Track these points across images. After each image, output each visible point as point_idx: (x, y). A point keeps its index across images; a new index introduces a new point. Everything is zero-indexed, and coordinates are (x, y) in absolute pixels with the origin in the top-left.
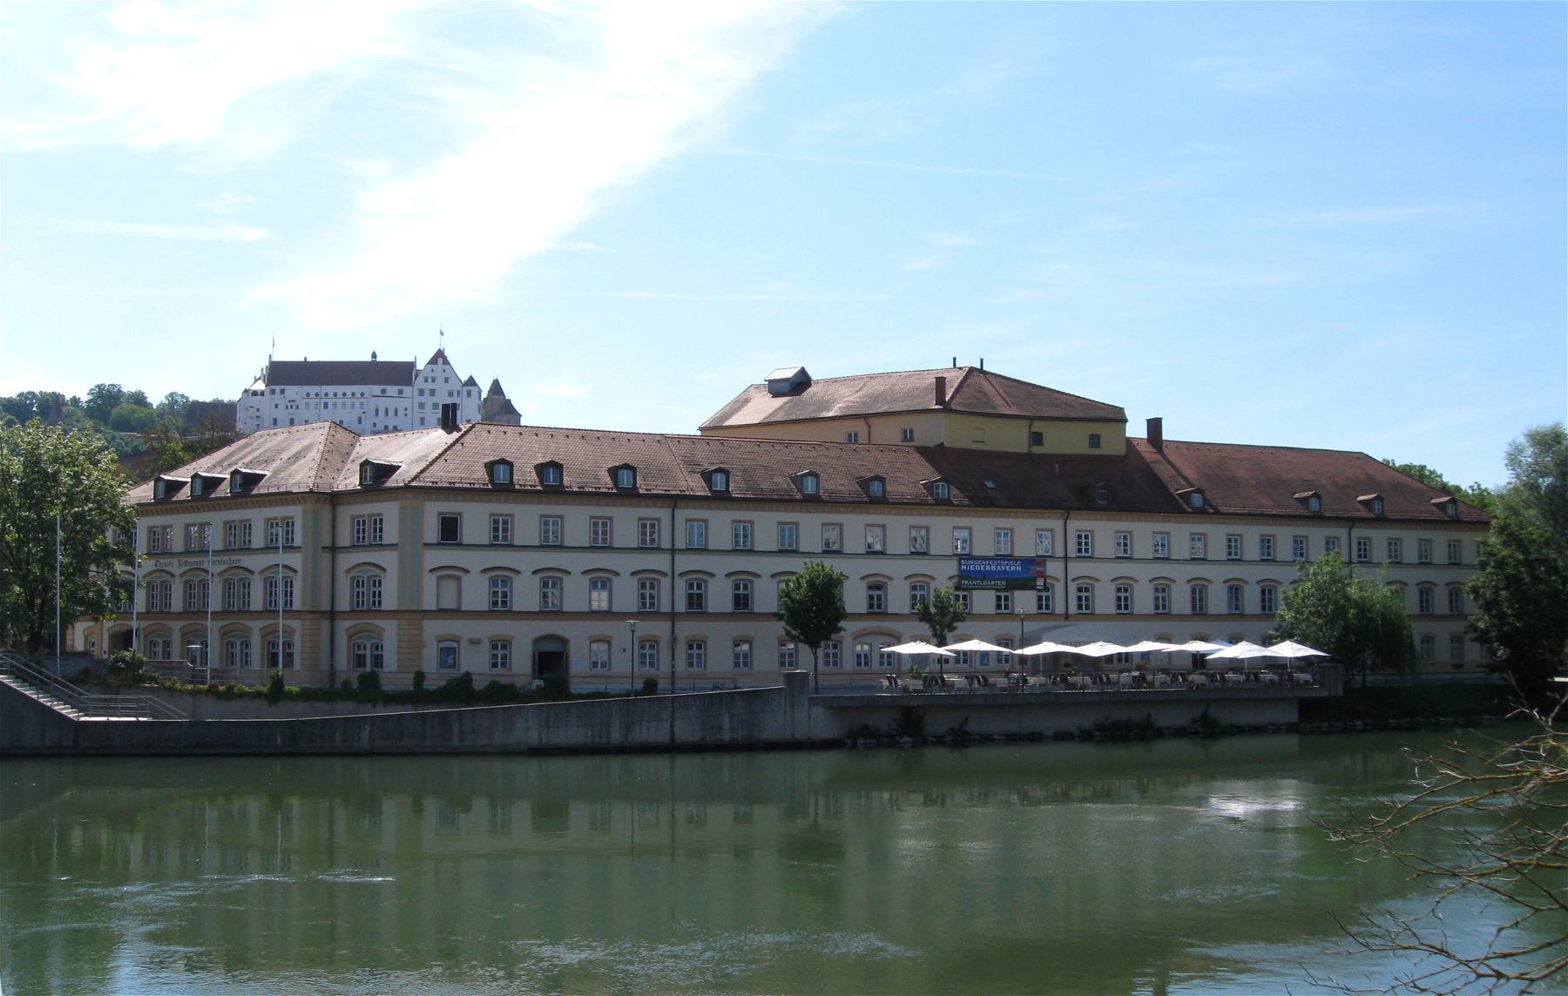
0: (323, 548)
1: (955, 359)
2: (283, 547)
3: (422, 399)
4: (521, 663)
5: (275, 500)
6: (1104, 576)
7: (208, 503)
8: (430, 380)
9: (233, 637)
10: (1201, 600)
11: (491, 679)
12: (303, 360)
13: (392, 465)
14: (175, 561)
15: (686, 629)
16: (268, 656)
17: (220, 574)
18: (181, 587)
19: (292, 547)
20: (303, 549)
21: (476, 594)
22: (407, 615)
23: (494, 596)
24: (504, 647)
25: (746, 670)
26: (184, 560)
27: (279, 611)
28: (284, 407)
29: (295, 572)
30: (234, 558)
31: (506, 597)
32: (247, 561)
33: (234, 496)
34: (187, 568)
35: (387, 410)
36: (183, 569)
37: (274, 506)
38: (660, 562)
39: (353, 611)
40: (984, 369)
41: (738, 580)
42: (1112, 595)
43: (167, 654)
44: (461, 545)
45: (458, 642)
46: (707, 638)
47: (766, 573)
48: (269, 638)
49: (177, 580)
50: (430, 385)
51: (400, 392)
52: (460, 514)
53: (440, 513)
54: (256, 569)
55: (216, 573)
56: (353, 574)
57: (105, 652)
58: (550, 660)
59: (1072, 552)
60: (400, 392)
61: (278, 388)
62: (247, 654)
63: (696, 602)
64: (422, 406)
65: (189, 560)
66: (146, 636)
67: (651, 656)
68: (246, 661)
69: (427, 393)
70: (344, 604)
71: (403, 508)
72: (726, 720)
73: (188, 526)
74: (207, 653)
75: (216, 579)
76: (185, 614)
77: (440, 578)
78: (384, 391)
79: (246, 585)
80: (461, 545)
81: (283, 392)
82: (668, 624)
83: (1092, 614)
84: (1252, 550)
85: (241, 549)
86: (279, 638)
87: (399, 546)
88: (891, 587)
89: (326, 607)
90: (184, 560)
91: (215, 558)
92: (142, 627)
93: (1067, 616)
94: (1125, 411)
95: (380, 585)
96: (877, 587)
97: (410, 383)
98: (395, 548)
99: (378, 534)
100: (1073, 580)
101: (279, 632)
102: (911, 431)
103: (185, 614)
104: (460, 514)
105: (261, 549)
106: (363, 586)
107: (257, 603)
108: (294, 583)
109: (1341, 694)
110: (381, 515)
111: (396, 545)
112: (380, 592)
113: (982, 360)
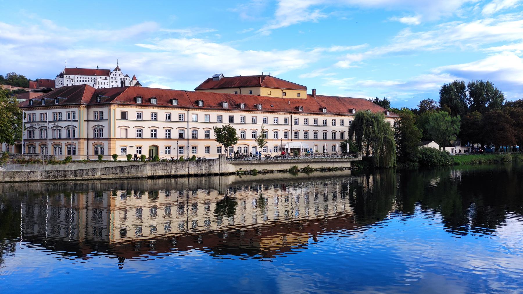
0: (85, 120)
1: (263, 73)
3: (112, 80)
4: (146, 152)
6: (301, 129)
8: (115, 75)
10: (334, 135)
12: (75, 68)
15: (192, 143)
16: (67, 151)
17: (51, 128)
19: (75, 120)
21: (132, 133)
23: (137, 134)
24: (195, 148)
25: (208, 154)
26: (39, 124)
27: (71, 139)
28: (70, 81)
29: (76, 127)
31: (141, 134)
32: (60, 124)
34: (41, 126)
35: (102, 83)
36: (39, 126)
37: (69, 108)
38: (185, 125)
40: (271, 75)
41: (138, 129)
42: (303, 134)
44: (127, 120)
47: (201, 128)
50: (115, 76)
51: (106, 78)
52: (127, 112)
53: (121, 111)
54: (63, 127)
55: (50, 128)
58: (154, 151)
59: (293, 123)
60: (106, 78)
61: (68, 76)
62: (60, 151)
63: (195, 136)
64: (112, 82)
65: (41, 124)
67: (220, 150)
68: (60, 153)
69: (114, 78)
70: (91, 136)
72: (203, 168)
76: (94, 139)
78: (101, 78)
79: (60, 131)
81: (69, 77)
82: (187, 142)
83: (157, 138)
84: (338, 123)
86: (71, 146)
88: (247, 132)
91: (49, 123)
93: (292, 140)
95: (103, 131)
96: (334, 134)
97: (108, 75)
100: (190, 129)
101: (71, 144)
102: (252, 91)
104: (127, 112)
105: (52, 121)
106: (97, 131)
107: (64, 136)
108: (76, 130)
109: (361, 160)
111: (108, 120)
112: (103, 133)
113: (270, 73)
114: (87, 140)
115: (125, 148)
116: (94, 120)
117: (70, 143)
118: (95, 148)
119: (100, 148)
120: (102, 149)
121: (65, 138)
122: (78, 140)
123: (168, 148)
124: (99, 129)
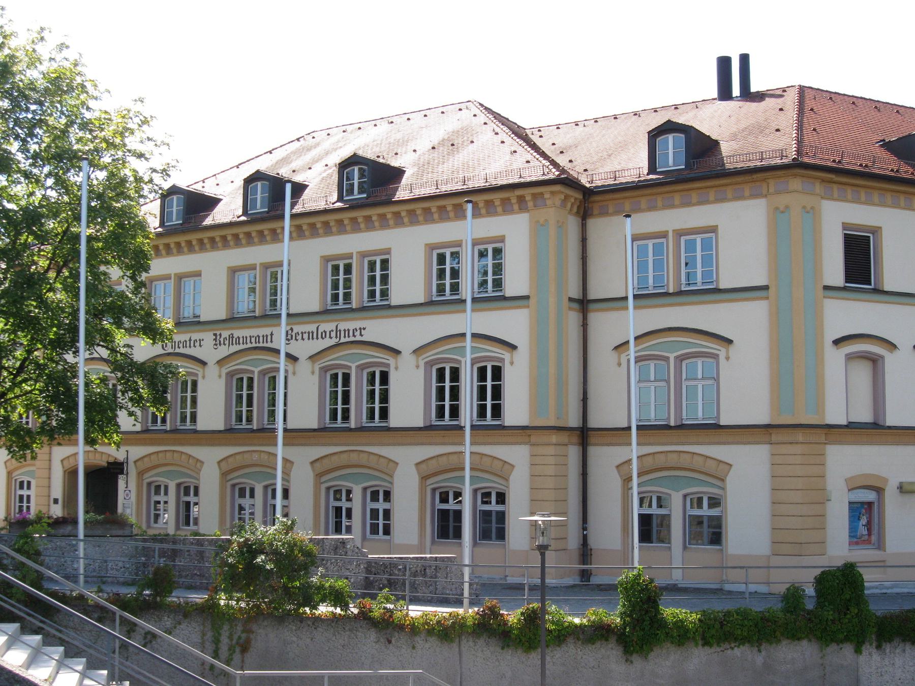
2: (474, 300)
5: (224, 238)
7: (200, 235)
9: (157, 475)
11: (822, 570)
13: (389, 166)
14: (208, 337)
18: (419, 376)
20: (532, 301)
22: (800, 436)
26: (226, 334)
30: (351, 325)
33: (168, 231)
36: (224, 351)
39: (229, 430)
43: (185, 515)
44: (878, 291)
45: (879, 491)
46: (886, 480)
48: (331, 480)
49: (212, 370)
52: (876, 231)
53: (845, 226)
56: (431, 355)
57: (56, 501)
65: (237, 333)
66: (141, 474)
71: (776, 212)
73: (233, 271)
74: (274, 506)
75: (304, 366)
76: (228, 434)
77: (850, 357)
80: (878, 291)
85: (234, 318)
87: (772, 291)
89: (574, 421)
90: (226, 334)
92: (132, 459)
94: (246, 177)
98: (762, 294)
99: (378, 288)
103: (228, 434)
104: (876, 231)
105: (421, 304)
110: (388, 251)
111: (766, 288)
114: (575, 439)
115: (871, 496)
116: (430, 303)
117: (454, 459)
118: (328, 489)
119: (365, 489)
120: (187, 493)
121: (422, 426)
122: (774, 438)
123: (494, 498)
124: (361, 368)
